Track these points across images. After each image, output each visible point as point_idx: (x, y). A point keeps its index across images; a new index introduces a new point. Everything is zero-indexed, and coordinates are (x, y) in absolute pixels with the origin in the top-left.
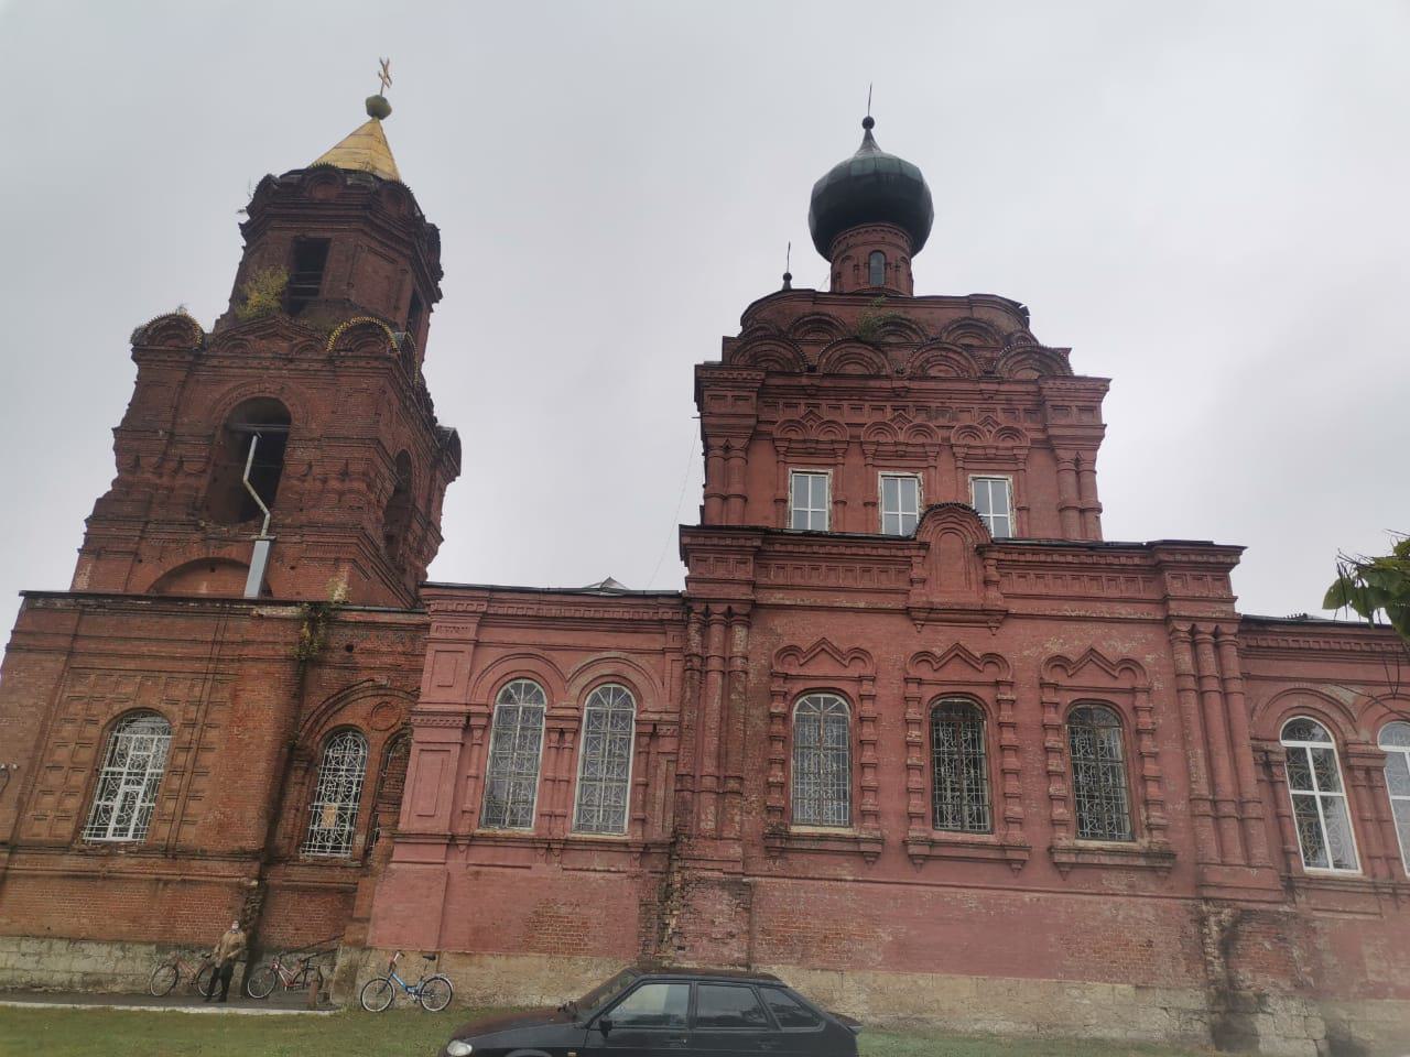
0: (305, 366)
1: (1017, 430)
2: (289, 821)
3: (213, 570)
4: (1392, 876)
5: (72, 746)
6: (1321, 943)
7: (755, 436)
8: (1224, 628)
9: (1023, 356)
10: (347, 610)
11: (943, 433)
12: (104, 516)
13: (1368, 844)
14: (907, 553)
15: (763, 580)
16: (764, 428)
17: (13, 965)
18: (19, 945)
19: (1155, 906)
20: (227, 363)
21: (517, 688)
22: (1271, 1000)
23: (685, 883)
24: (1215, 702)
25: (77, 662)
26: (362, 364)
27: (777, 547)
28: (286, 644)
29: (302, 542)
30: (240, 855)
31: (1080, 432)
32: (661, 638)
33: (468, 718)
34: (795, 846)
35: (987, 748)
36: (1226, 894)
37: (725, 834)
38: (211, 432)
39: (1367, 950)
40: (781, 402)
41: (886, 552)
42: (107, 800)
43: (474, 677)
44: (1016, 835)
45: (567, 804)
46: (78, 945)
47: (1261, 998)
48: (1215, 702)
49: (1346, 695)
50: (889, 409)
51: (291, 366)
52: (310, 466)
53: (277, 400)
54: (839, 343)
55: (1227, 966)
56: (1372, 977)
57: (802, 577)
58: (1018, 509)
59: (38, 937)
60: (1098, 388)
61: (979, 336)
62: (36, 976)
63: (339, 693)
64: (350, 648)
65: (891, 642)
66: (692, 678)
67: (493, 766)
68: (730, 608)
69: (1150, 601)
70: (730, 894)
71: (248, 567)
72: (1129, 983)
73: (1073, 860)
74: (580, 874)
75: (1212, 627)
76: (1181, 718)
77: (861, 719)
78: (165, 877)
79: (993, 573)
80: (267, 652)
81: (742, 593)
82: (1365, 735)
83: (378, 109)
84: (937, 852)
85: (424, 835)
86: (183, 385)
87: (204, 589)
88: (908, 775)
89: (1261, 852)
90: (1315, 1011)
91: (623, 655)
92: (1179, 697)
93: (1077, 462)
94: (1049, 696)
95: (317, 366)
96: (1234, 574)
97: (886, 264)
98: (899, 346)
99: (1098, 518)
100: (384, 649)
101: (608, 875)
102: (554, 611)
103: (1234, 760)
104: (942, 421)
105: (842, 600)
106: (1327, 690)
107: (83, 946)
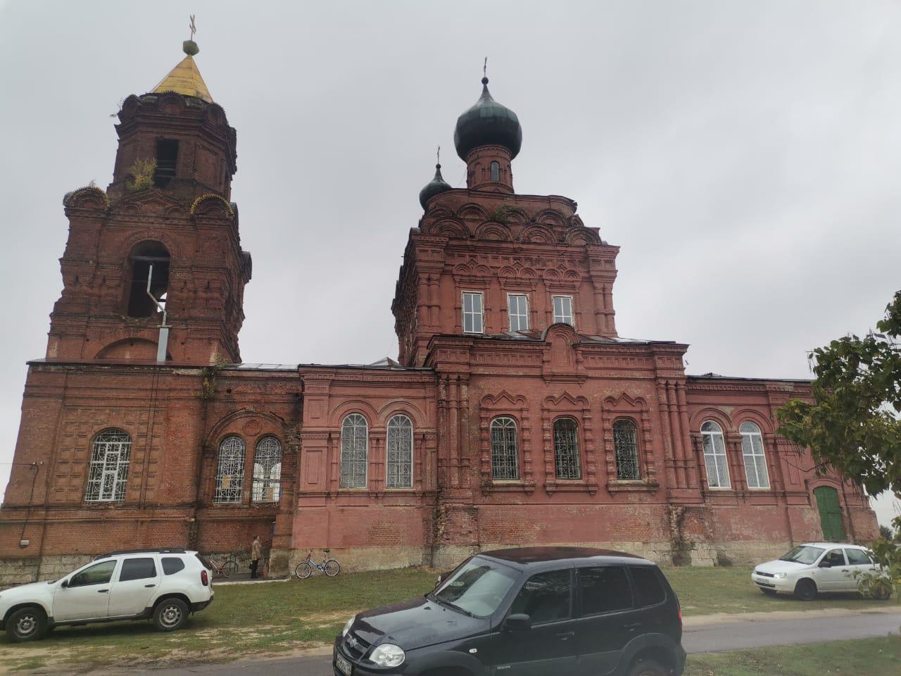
0: (176, 222)
1: (576, 272)
2: (206, 486)
3: (132, 345)
4: (743, 489)
5: (73, 450)
6: (715, 519)
7: (444, 273)
8: (680, 382)
9: (578, 232)
10: (227, 370)
11: (539, 273)
12: (60, 313)
14: (541, 348)
15: (473, 362)
16: (447, 268)
18: (61, 560)
19: (651, 508)
20: (127, 219)
21: (352, 417)
23: (447, 510)
24: (675, 415)
25: (68, 402)
26: (213, 222)
27: (480, 345)
28: (195, 390)
29: (187, 329)
31: (606, 274)
32: (423, 391)
33: (330, 435)
34: (496, 490)
35: (579, 440)
36: (679, 501)
37: (464, 486)
38: (121, 262)
39: (732, 521)
41: (532, 348)
42: (97, 479)
43: (330, 413)
44: (592, 480)
45: (383, 475)
47: (693, 544)
48: (675, 415)
49: (728, 410)
50: (512, 259)
51: (168, 222)
52: (185, 283)
53: (160, 243)
54: (486, 222)
55: (680, 531)
56: (734, 532)
57: (492, 360)
58: (576, 313)
59: (71, 555)
60: (614, 251)
61: (554, 219)
64: (229, 391)
65: (535, 392)
66: (443, 412)
67: (343, 458)
68: (459, 377)
70: (468, 514)
71: (157, 344)
72: (640, 541)
73: (617, 490)
74: (392, 508)
75: (674, 382)
76: (661, 423)
77: (523, 429)
79: (580, 356)
81: (464, 369)
82: (734, 428)
83: (191, 49)
84: (559, 489)
85: (314, 493)
86: (100, 232)
88: (545, 455)
89: (694, 482)
90: (713, 547)
91: (405, 400)
93: (604, 289)
94: (606, 416)
96: (684, 357)
97: (499, 169)
98: (515, 224)
99: (613, 319)
100: (249, 391)
101: (406, 508)
102: (370, 378)
103: (683, 441)
104: (538, 266)
105: (512, 372)
106: (720, 408)
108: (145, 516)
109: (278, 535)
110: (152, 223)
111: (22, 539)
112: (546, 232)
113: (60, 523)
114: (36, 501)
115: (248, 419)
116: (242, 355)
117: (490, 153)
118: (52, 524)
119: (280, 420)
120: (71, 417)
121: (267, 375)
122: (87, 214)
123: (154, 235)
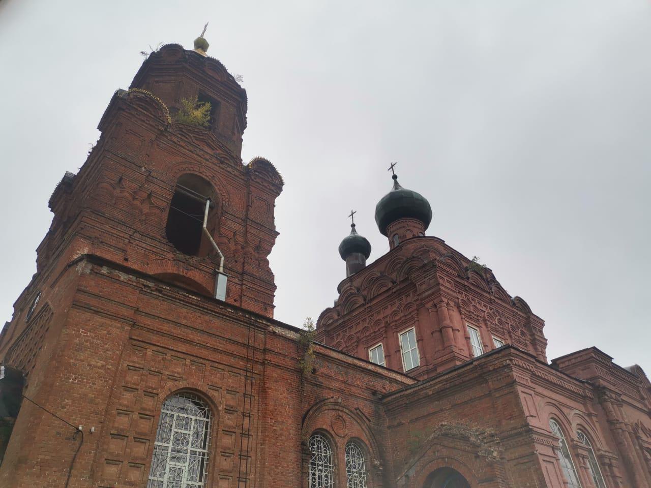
0: (229, 169)
5: (136, 416)
51: (221, 165)
63: (157, 372)
95: (236, 173)
110: (207, 160)
116: (511, 295)
120: (136, 360)
123: (206, 174)
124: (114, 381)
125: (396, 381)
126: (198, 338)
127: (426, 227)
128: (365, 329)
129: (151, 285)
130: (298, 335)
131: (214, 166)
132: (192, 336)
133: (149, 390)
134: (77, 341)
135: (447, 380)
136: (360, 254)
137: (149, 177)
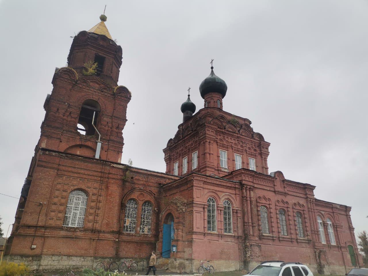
0: (106, 94)
5: (60, 198)
11: (245, 148)
13: (327, 239)
17: (50, 264)
20: (84, 87)
22: (325, 266)
30: (113, 232)
34: (285, 240)
40: (218, 134)
46: (70, 257)
49: (323, 213)
51: (102, 93)
52: (108, 123)
58: (256, 166)
59: (57, 255)
62: (58, 267)
64: (132, 178)
69: (303, 194)
70: (258, 248)
78: (93, 238)
80: (115, 177)
87: (78, 153)
91: (229, 194)
92: (309, 212)
95: (109, 95)
96: (314, 191)
107: (72, 258)
108: (95, 236)
109: (180, 252)
110: (95, 92)
111: (32, 245)
112: (247, 132)
113: (52, 237)
114: (40, 224)
115: (139, 193)
117: (217, 96)
118: (48, 237)
119: (154, 195)
120: (60, 180)
121: (149, 173)
122: (66, 80)
123: (95, 98)
124: (52, 189)
125: (172, 179)
126: (82, 171)
127: (119, 152)
128: (182, 150)
129: (64, 155)
130: (124, 167)
131: (98, 94)
132: (79, 171)
133: (64, 190)
134: (39, 177)
135: (179, 182)
136: (189, 111)
137: (69, 106)
